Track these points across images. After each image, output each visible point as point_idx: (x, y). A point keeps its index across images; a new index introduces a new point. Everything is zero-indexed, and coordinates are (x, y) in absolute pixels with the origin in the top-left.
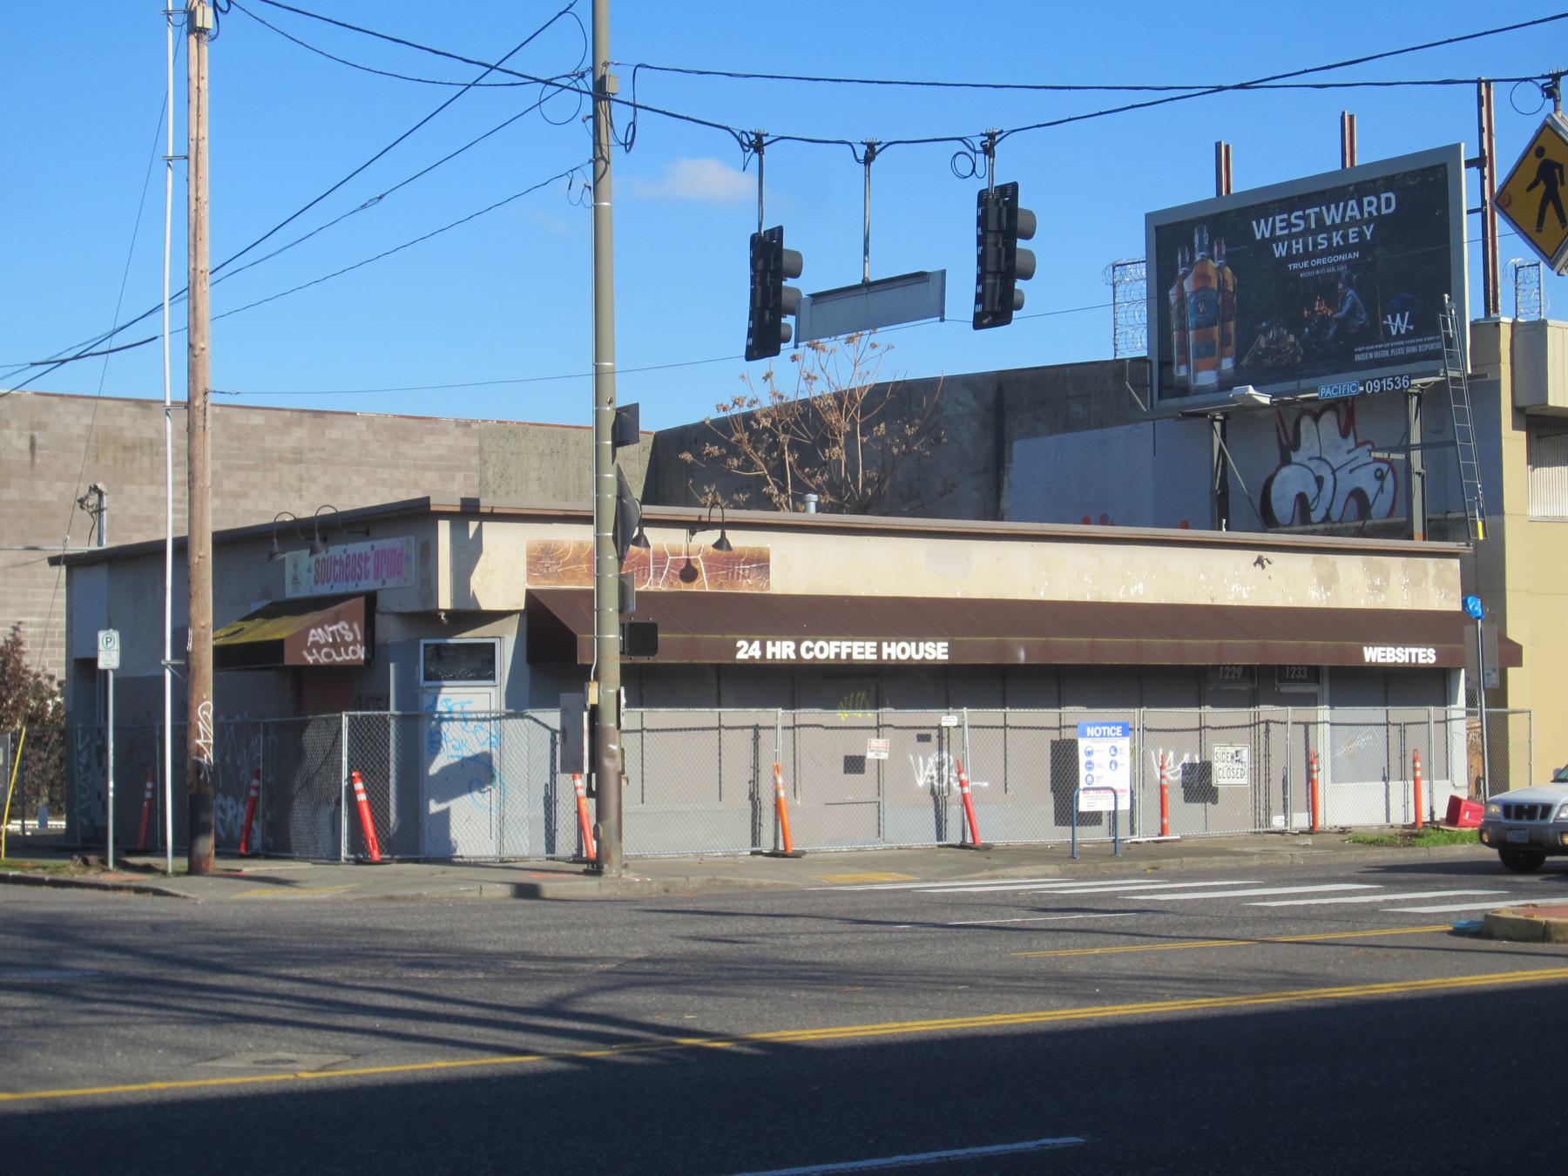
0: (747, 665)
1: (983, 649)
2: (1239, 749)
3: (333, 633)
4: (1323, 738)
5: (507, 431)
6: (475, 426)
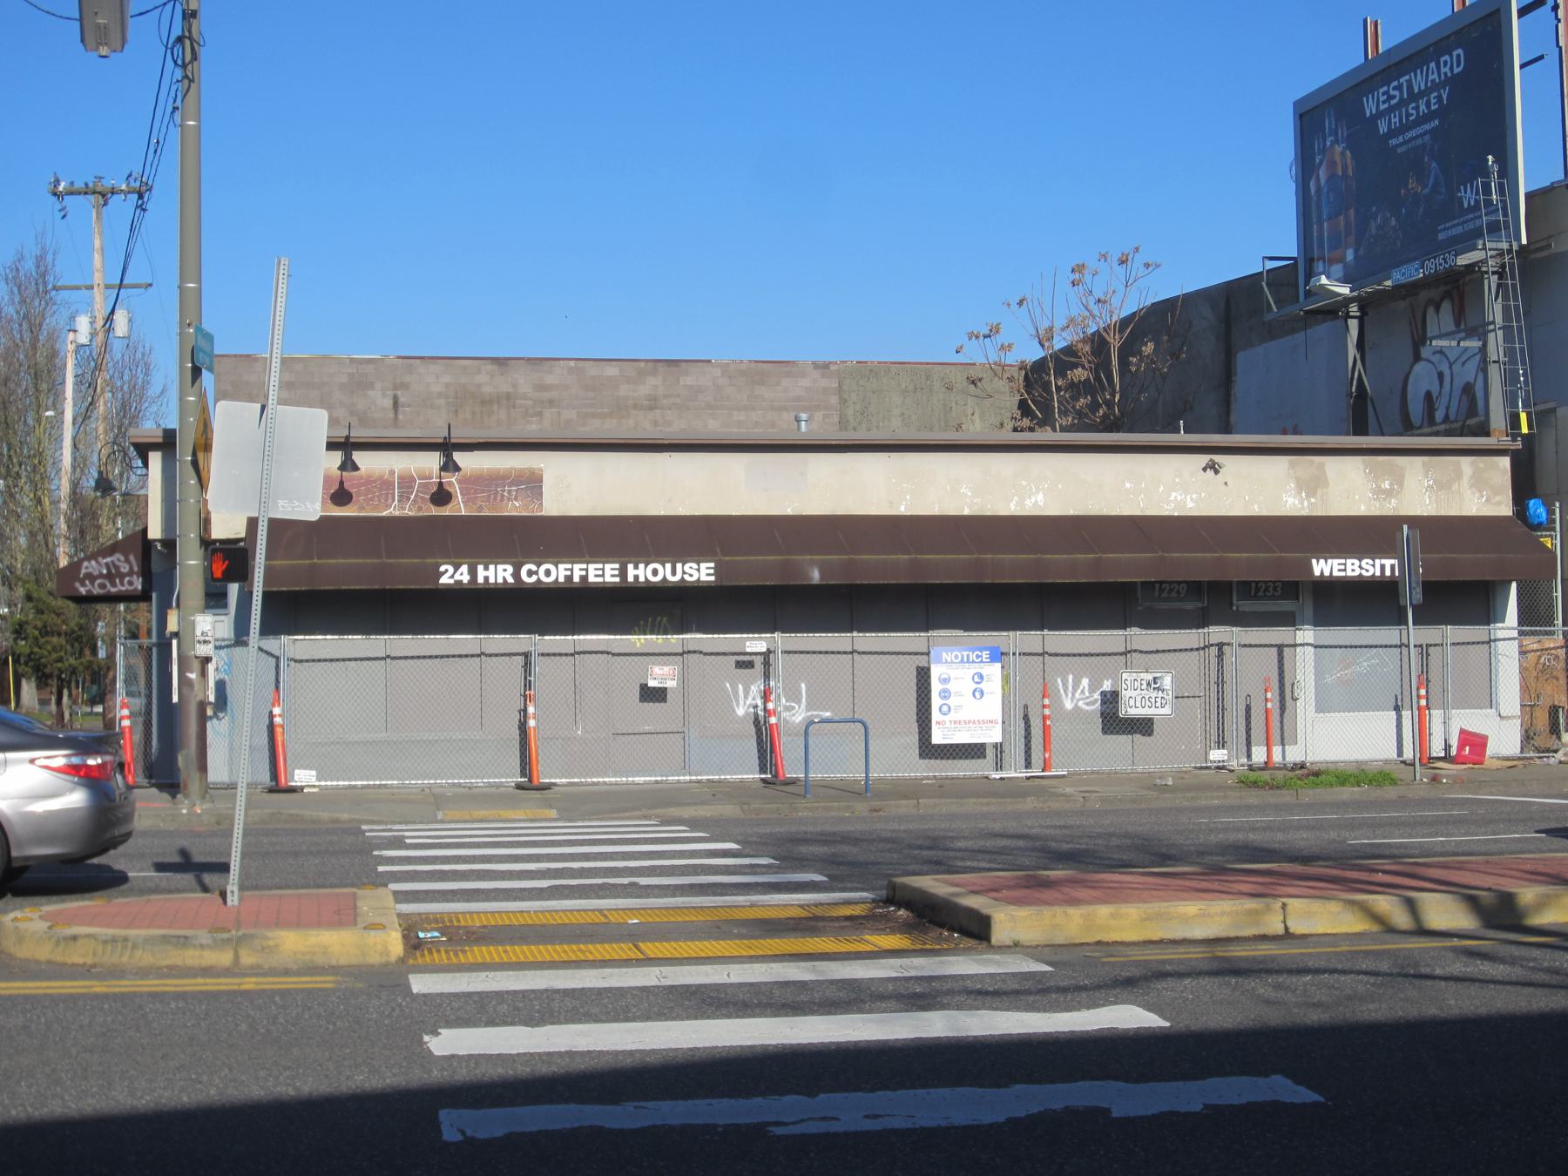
0: (456, 590)
1: (760, 567)
2: (1158, 675)
3: (107, 565)
4: (1304, 664)
5: (866, 371)
6: (833, 368)
